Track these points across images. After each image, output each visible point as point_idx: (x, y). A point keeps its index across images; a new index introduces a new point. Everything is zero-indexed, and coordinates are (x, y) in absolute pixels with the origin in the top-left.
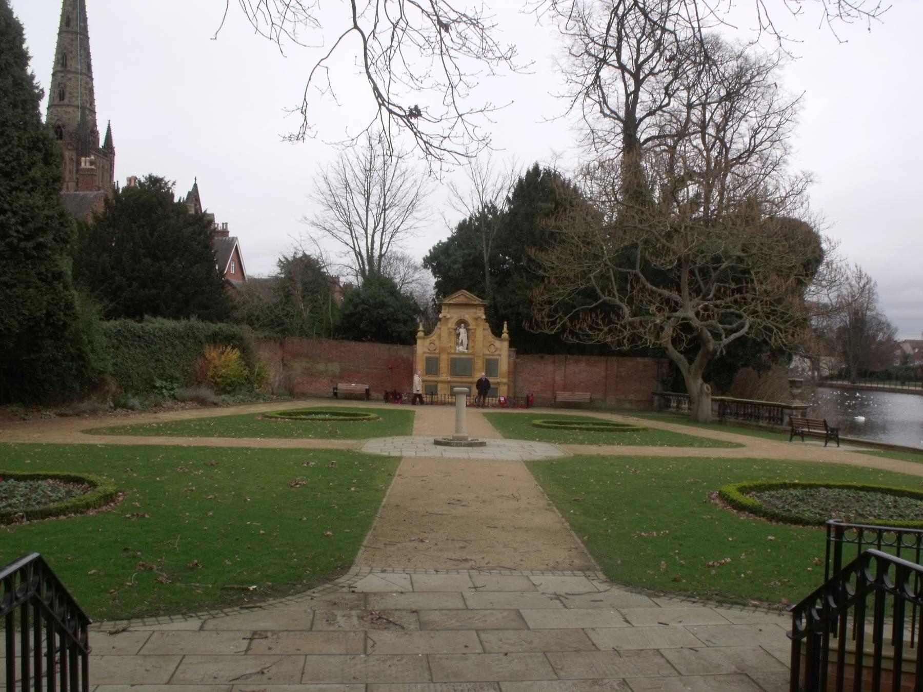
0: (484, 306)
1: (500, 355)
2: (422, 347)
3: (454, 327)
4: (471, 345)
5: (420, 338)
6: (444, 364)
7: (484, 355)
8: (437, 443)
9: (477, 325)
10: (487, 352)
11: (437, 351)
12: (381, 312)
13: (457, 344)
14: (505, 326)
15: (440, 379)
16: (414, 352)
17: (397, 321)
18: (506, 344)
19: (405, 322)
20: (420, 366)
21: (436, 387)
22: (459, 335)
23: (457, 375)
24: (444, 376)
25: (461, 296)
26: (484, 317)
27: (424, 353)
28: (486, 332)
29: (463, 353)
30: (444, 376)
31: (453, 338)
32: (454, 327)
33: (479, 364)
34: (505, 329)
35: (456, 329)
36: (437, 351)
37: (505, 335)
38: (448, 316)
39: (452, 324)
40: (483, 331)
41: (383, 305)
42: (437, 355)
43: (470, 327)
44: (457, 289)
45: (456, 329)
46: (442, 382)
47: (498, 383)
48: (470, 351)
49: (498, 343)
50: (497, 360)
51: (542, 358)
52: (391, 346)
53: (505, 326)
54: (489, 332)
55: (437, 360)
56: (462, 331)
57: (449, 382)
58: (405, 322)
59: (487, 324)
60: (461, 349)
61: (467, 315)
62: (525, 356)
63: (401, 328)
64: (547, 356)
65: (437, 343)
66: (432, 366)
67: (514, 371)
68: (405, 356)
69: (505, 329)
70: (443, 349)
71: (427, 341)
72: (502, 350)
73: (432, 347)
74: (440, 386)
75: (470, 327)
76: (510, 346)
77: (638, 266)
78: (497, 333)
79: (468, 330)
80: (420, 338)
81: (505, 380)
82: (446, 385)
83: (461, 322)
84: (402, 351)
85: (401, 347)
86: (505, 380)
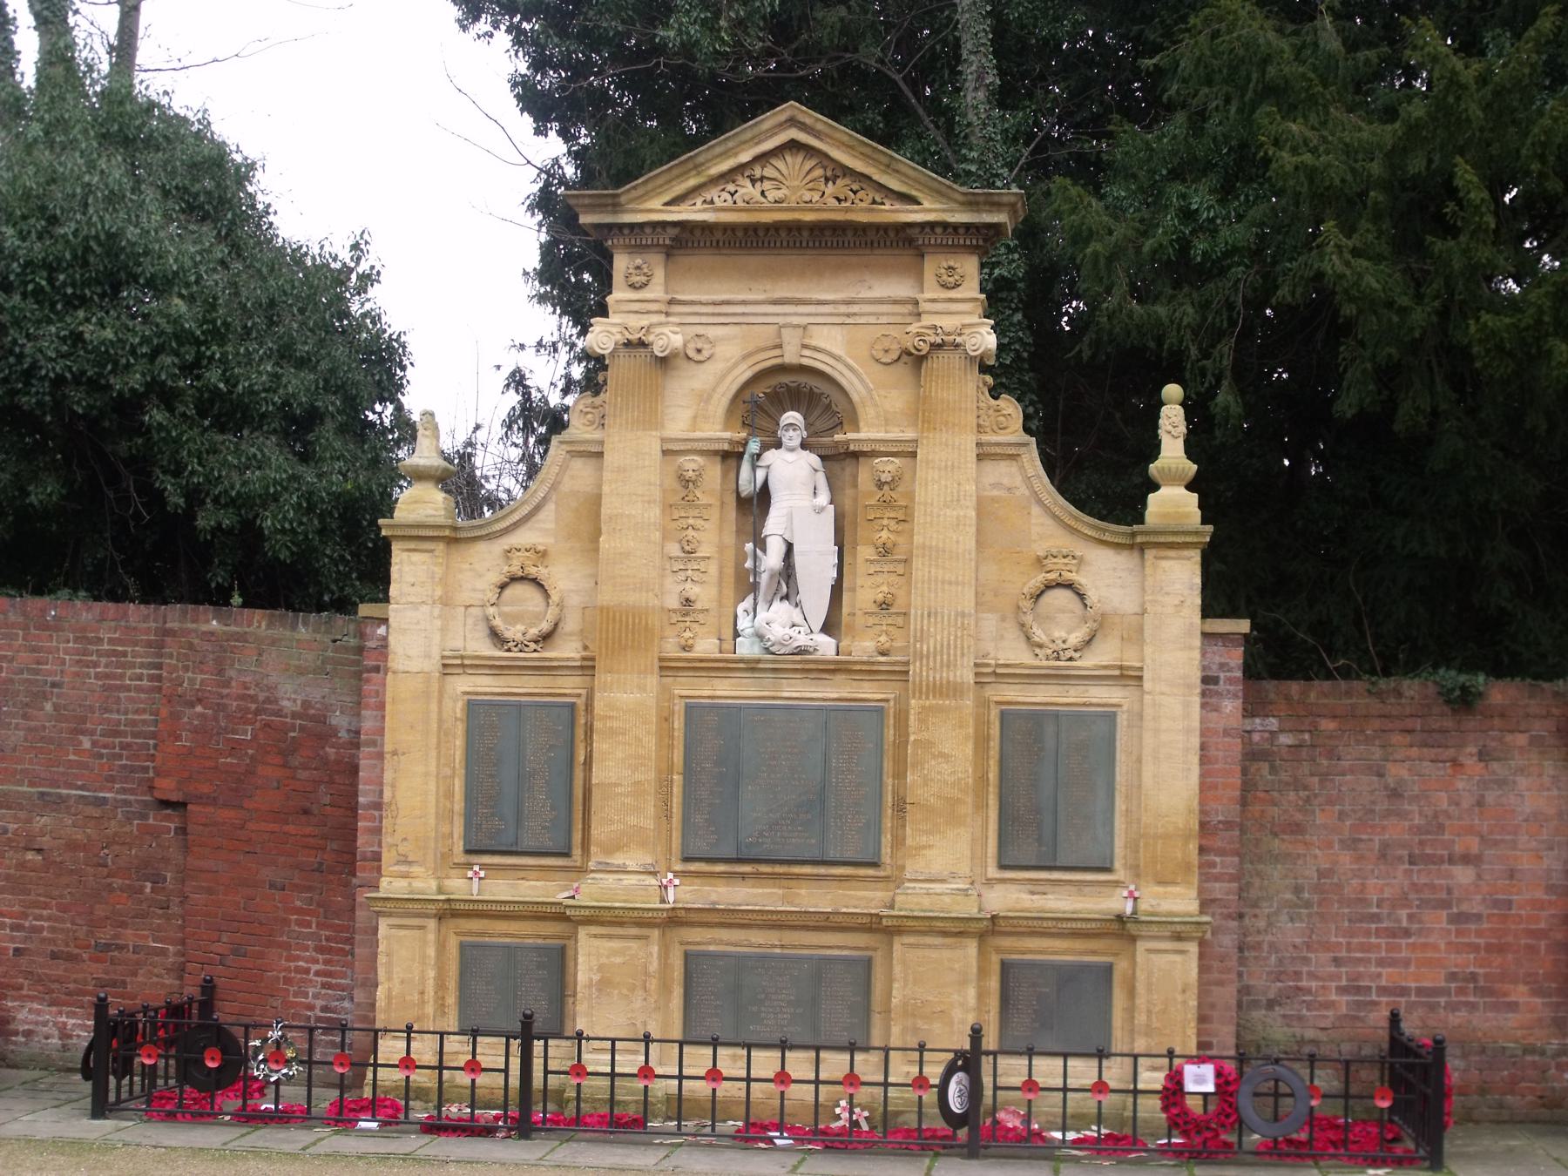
0: (980, 239)
1: (1129, 677)
2: (430, 615)
3: (718, 432)
4: (864, 594)
5: (421, 535)
6: (629, 761)
7: (989, 674)
8: (790, 547)
9: (923, 413)
10: (1014, 653)
11: (567, 650)
12: (98, 331)
13: (747, 585)
14: (1172, 421)
15: (593, 890)
16: (364, 665)
17: (230, 413)
18: (1182, 576)
19: (298, 427)
20: (416, 787)
21: (558, 962)
22: (757, 503)
23: (746, 859)
24: (631, 863)
25: (777, 164)
26: (986, 339)
27: (452, 665)
28: (1002, 472)
29: (802, 663)
30: (631, 863)
31: (713, 533)
32: (718, 432)
33: (948, 757)
34: (1172, 452)
35: (731, 456)
36: (567, 650)
37: (1173, 502)
38: (668, 338)
39: (696, 408)
40: (974, 472)
41: (110, 272)
42: (570, 685)
43: (867, 433)
44: (730, 105)
45: (731, 456)
46: (606, 919)
47: (1123, 929)
48: (863, 647)
49: (1106, 572)
50: (1109, 717)
51: (1464, 701)
52: (174, 616)
53: (1172, 421)
54: (1025, 474)
55: (569, 726)
56: (791, 470)
57: (674, 920)
58: (298, 427)
59: (1011, 409)
60: (778, 622)
61: (840, 324)
62: (1317, 692)
63: (261, 463)
64: (1499, 693)
65: (564, 578)
66: (526, 780)
67: (1242, 826)
68: (290, 695)
69: (1172, 452)
70: (616, 633)
71: (482, 566)
72: (1143, 620)
73: (524, 614)
74: (592, 956)
75: (867, 433)
76: (1216, 600)
77: (1117, 865)
78: (1098, 474)
79: (838, 461)
80: (421, 535)
81: (1181, 901)
82: (648, 952)
83: (785, 394)
84: (274, 656)
85: (258, 622)
86: (1181, 901)
